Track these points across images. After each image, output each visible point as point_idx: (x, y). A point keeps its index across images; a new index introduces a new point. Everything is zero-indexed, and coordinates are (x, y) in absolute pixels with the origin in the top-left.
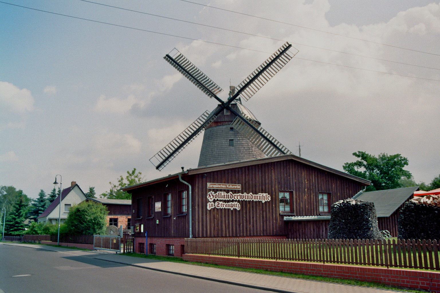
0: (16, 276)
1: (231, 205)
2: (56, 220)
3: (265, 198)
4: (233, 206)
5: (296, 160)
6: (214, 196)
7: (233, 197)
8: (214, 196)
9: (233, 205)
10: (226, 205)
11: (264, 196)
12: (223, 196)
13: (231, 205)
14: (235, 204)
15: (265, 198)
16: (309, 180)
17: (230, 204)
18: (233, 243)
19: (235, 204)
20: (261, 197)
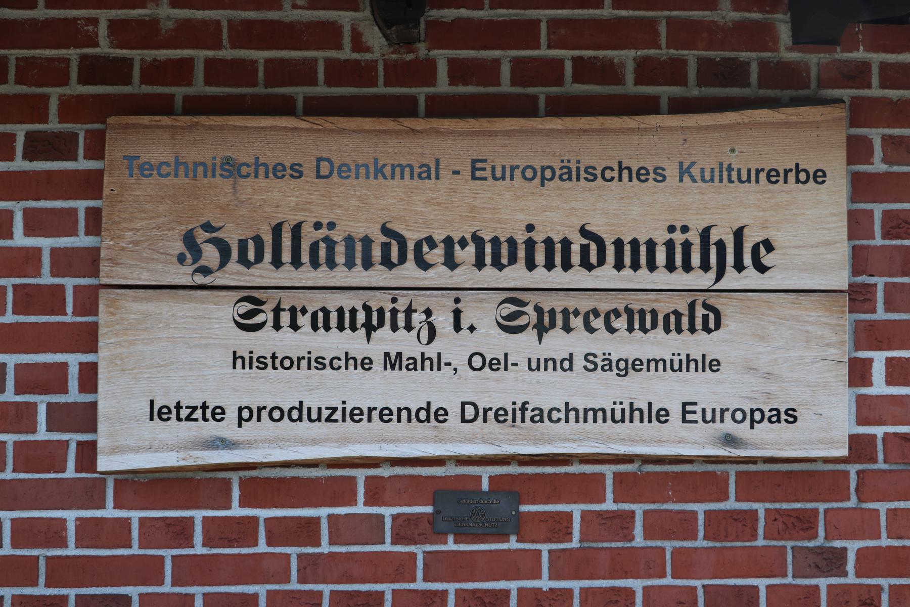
0: (600, 545)
1: (361, 317)
2: (297, 5)
3: (730, 259)
4: (375, 322)
5: (176, 48)
6: (235, 254)
7: (411, 256)
8: (235, 254)
9: (381, 311)
10: (314, 316)
11: (721, 245)
12: (314, 248)
13: (361, 317)
14: (394, 312)
15: (730, 259)
16: (521, 221)
17: (353, 312)
18: (212, 444)
19: (394, 312)
20: (687, 246)
